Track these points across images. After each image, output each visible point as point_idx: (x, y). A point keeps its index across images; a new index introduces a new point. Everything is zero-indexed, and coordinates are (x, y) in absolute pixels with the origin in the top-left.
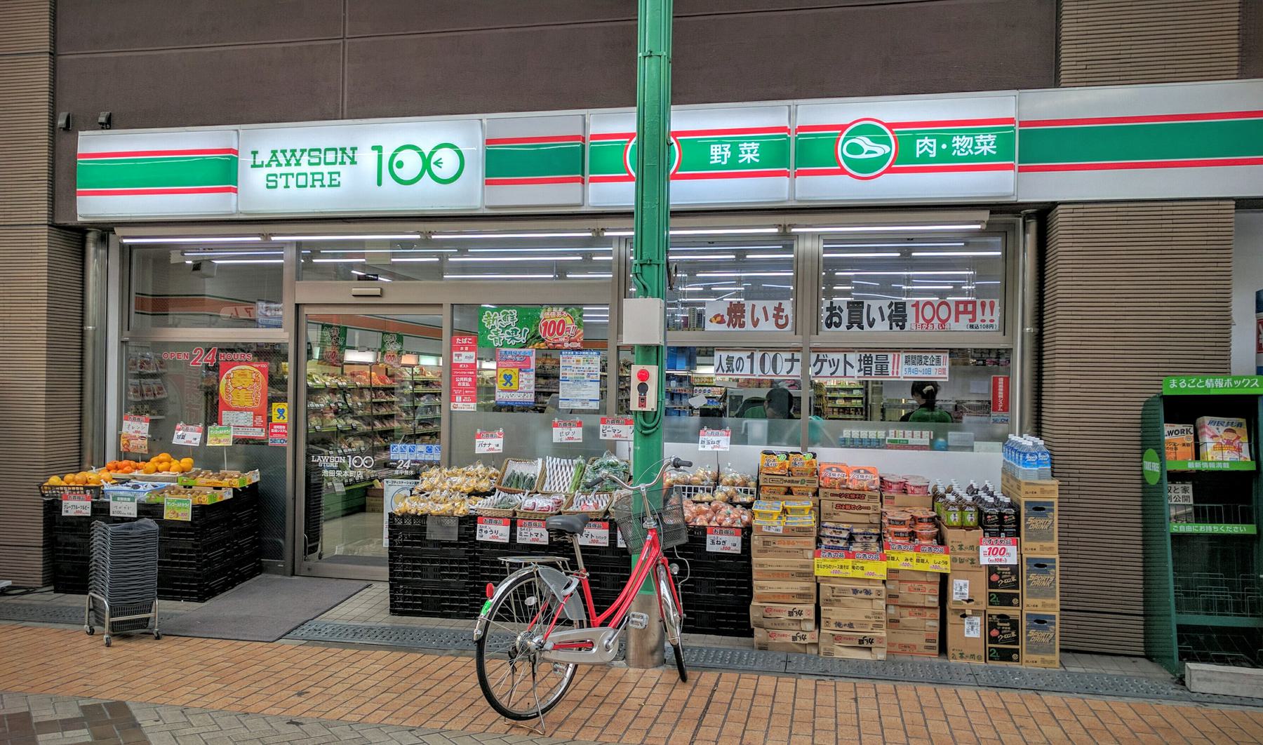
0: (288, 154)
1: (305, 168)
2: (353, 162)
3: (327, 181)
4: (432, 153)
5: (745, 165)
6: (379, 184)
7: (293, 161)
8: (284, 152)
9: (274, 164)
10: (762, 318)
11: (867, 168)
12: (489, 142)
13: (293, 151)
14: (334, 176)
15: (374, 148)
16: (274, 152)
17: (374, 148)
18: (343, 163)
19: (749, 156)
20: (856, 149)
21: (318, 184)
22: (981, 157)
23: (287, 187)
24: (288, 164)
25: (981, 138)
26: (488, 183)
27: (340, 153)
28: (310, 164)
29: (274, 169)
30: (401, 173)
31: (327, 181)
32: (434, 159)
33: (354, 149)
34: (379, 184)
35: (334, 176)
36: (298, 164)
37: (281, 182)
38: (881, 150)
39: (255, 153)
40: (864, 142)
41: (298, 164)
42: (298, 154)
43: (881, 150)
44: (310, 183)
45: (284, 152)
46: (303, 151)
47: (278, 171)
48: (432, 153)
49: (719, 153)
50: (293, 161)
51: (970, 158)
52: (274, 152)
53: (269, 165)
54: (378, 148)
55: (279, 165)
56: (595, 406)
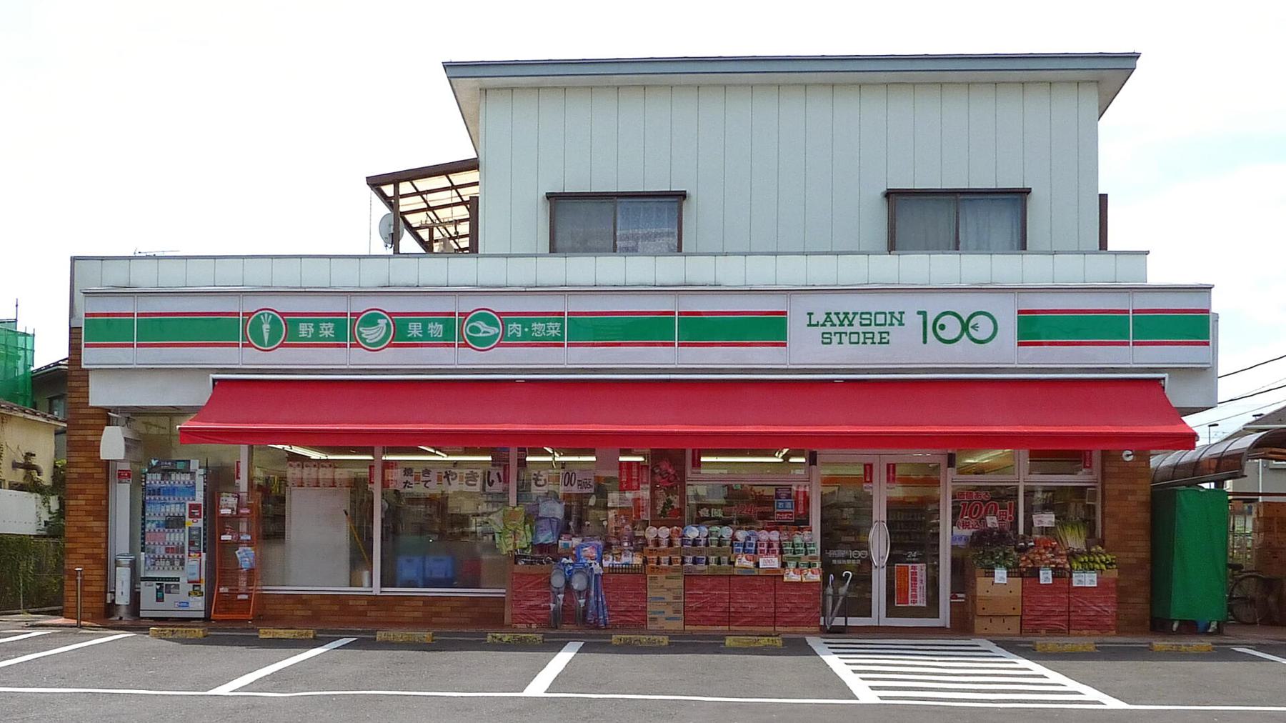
0: (842, 317)
1: (857, 327)
2: (901, 324)
3: (877, 339)
4: (969, 320)
5: (324, 338)
6: (925, 342)
7: (846, 322)
8: (837, 314)
9: (828, 324)
10: (496, 479)
11: (483, 343)
12: (1020, 312)
13: (846, 314)
15: (919, 313)
16: (828, 314)
17: (919, 313)
18: (891, 324)
19: (553, 332)
20: (477, 330)
21: (869, 341)
22: (551, 338)
23: (840, 343)
24: (842, 325)
25: (550, 325)
26: (1020, 344)
27: (889, 316)
28: (862, 325)
29: (828, 328)
30: (941, 334)
31: (877, 339)
32: (939, 323)
33: (902, 313)
34: (925, 342)
36: (851, 324)
37: (836, 339)
38: (493, 331)
39: (810, 314)
40: (481, 325)
41: (851, 324)
42: (851, 317)
43: (493, 331)
44: (862, 340)
45: (837, 314)
46: (855, 314)
47: (833, 330)
48: (969, 320)
49: (372, 334)
50: (846, 322)
51: (543, 338)
52: (828, 314)
53: (823, 325)
54: (924, 313)
55: (833, 325)
56: (202, 615)
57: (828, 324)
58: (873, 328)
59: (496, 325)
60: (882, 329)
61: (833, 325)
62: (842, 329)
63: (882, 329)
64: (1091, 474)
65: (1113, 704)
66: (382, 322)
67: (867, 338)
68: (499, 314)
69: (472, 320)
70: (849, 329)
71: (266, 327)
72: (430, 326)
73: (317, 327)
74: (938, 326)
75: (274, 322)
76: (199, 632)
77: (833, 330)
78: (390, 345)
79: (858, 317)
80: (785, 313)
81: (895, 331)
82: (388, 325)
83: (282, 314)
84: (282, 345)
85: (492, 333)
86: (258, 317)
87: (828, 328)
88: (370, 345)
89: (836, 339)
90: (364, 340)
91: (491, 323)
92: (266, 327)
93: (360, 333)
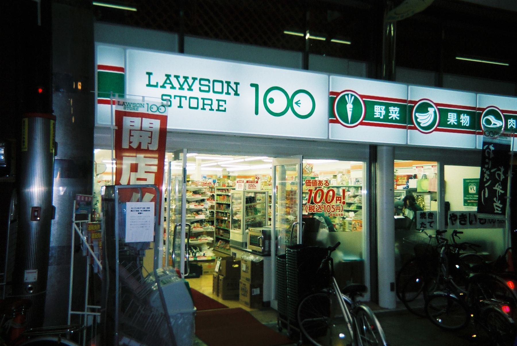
0: (182, 80)
1: (196, 93)
2: (236, 94)
6: (257, 113)
7: (186, 86)
8: (177, 77)
9: (168, 86)
13: (186, 78)
16: (168, 76)
17: (252, 85)
20: (488, 122)
24: (181, 88)
27: (225, 85)
28: (201, 90)
29: (168, 90)
31: (215, 106)
33: (237, 84)
34: (257, 113)
36: (190, 89)
39: (149, 74)
40: (491, 118)
41: (190, 89)
42: (190, 81)
44: (201, 106)
45: (177, 77)
46: (194, 79)
47: (173, 92)
50: (186, 86)
52: (168, 76)
53: (163, 87)
55: (173, 87)
57: (168, 86)
61: (173, 87)
64: (455, 233)
66: (431, 110)
68: (503, 111)
70: (189, 94)
71: (350, 107)
72: (462, 116)
73: (387, 111)
74: (268, 101)
75: (356, 102)
77: (173, 92)
78: (436, 130)
79: (197, 82)
80: (122, 69)
82: (435, 112)
83: (362, 97)
84: (362, 124)
85: (498, 125)
86: (343, 97)
87: (168, 90)
88: (423, 128)
90: (419, 124)
91: (498, 117)
92: (350, 107)
93: (416, 118)
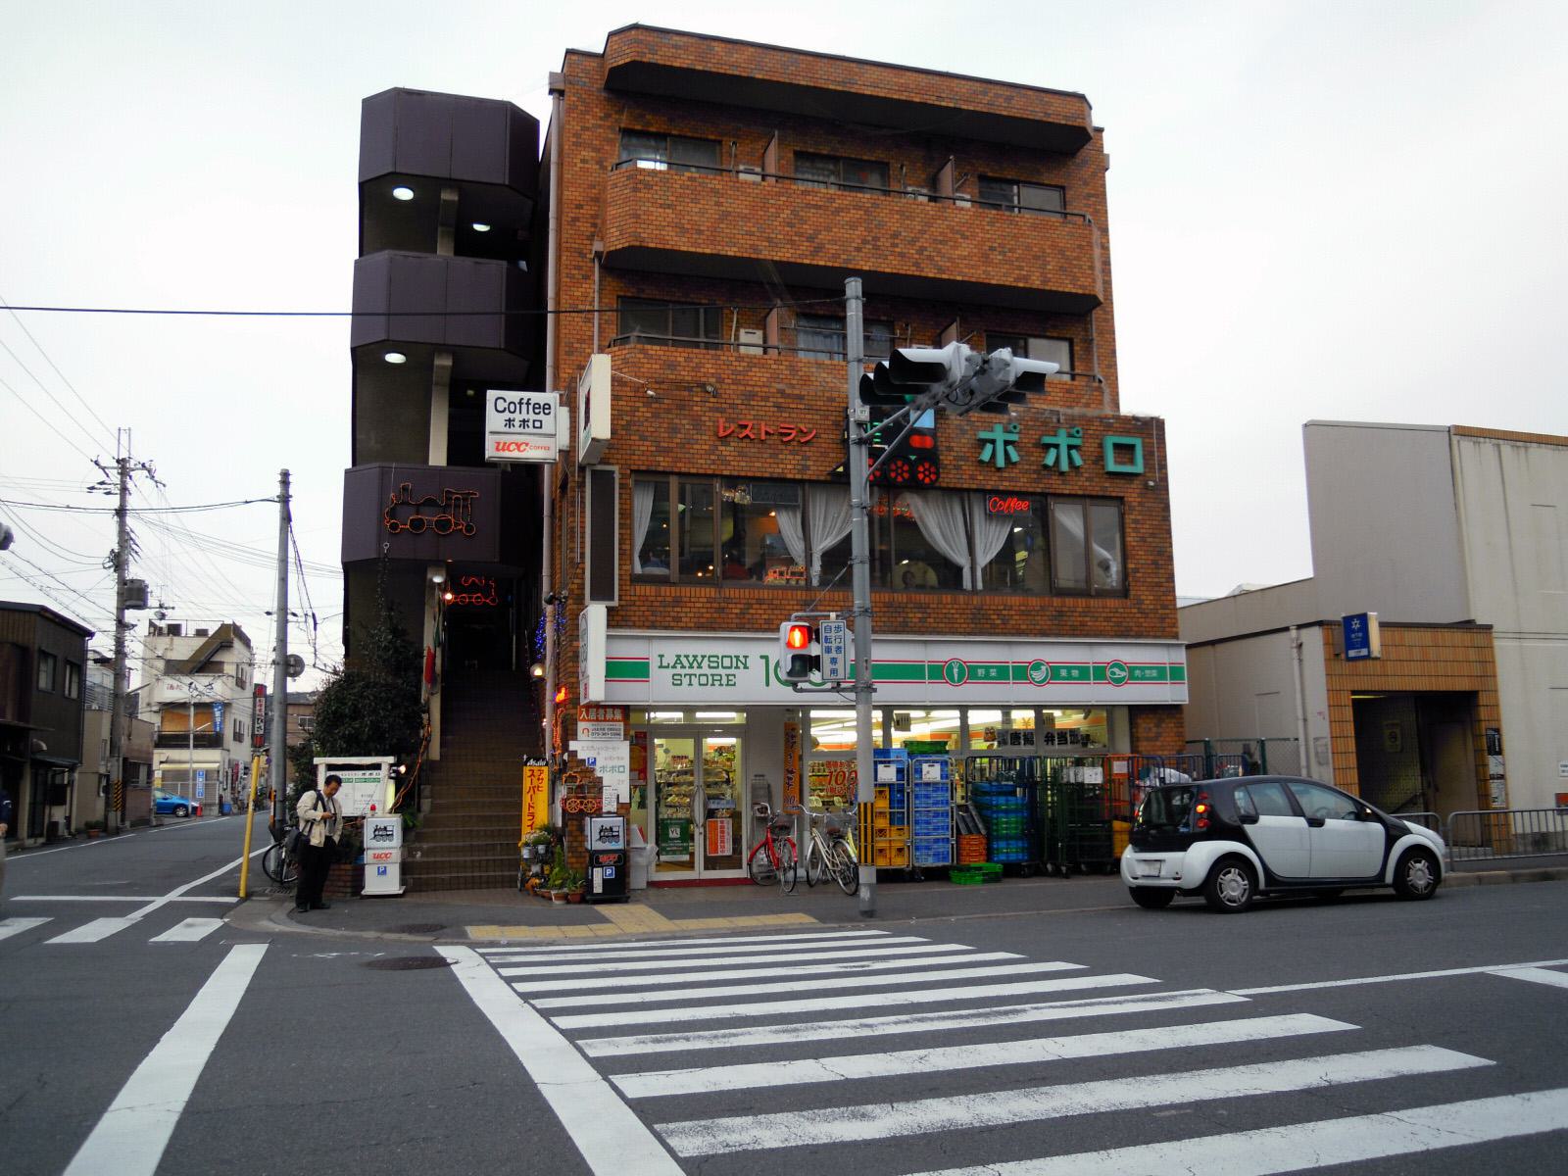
0: (691, 659)
1: (705, 670)
2: (746, 667)
3: (724, 681)
6: (768, 684)
8: (687, 657)
9: (679, 666)
13: (695, 657)
14: (730, 678)
15: (762, 657)
16: (678, 656)
17: (762, 657)
18: (737, 667)
20: (1113, 673)
24: (691, 667)
27: (734, 660)
28: (710, 667)
29: (679, 670)
31: (724, 681)
33: (746, 657)
34: (768, 684)
35: (730, 678)
36: (699, 667)
37: (686, 681)
38: (1123, 674)
39: (661, 656)
40: (1116, 670)
41: (699, 667)
42: (699, 659)
43: (1123, 674)
44: (710, 682)
45: (687, 657)
46: (703, 657)
47: (683, 672)
49: (1038, 676)
52: (678, 656)
53: (674, 667)
55: (683, 667)
58: (720, 671)
59: (1124, 670)
60: (729, 671)
61: (683, 667)
62: (691, 671)
63: (729, 671)
65: (1158, 981)
67: (715, 680)
69: (1111, 667)
70: (698, 672)
71: (956, 670)
76: (790, 927)
77: (683, 672)
79: (706, 659)
81: (740, 673)
87: (679, 670)
89: (686, 681)
90: (1033, 679)
92: (956, 670)
